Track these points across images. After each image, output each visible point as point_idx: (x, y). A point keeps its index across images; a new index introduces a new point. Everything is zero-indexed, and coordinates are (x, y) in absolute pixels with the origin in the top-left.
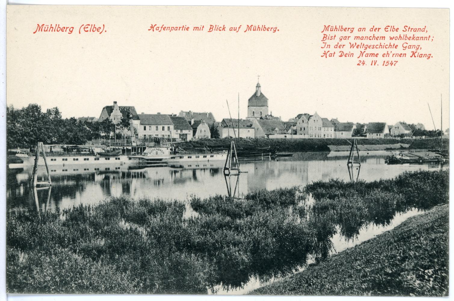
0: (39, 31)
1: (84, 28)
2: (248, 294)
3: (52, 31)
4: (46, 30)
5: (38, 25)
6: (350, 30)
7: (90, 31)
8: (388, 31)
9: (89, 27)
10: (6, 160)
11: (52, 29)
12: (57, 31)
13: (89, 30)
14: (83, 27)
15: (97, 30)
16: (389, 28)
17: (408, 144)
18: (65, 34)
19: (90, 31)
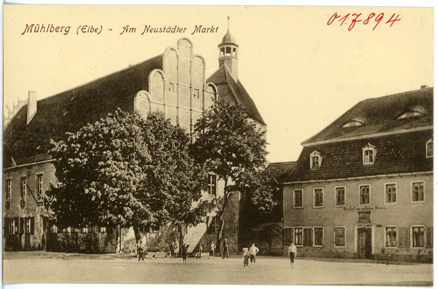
0: (28, 32)
1: (82, 29)
2: (354, 258)
3: (132, 32)
4: (36, 30)
5: (196, 26)
6: (64, 29)
7: (88, 32)
8: (85, 32)
9: (87, 28)
10: (2, 134)
11: (43, 29)
12: (91, 32)
13: (87, 31)
14: (81, 28)
15: (95, 30)
16: (87, 28)
17: (30, 237)
18: (61, 34)
19: (88, 32)
